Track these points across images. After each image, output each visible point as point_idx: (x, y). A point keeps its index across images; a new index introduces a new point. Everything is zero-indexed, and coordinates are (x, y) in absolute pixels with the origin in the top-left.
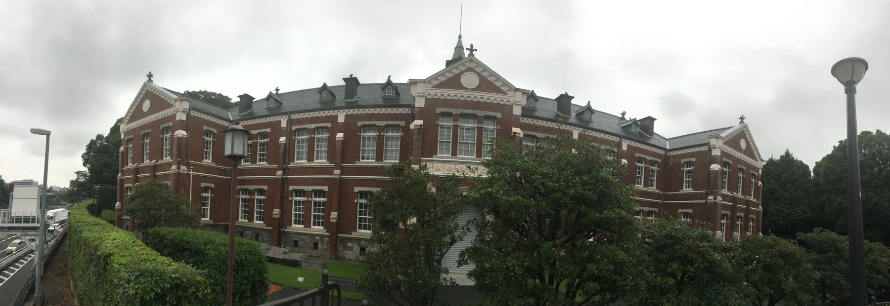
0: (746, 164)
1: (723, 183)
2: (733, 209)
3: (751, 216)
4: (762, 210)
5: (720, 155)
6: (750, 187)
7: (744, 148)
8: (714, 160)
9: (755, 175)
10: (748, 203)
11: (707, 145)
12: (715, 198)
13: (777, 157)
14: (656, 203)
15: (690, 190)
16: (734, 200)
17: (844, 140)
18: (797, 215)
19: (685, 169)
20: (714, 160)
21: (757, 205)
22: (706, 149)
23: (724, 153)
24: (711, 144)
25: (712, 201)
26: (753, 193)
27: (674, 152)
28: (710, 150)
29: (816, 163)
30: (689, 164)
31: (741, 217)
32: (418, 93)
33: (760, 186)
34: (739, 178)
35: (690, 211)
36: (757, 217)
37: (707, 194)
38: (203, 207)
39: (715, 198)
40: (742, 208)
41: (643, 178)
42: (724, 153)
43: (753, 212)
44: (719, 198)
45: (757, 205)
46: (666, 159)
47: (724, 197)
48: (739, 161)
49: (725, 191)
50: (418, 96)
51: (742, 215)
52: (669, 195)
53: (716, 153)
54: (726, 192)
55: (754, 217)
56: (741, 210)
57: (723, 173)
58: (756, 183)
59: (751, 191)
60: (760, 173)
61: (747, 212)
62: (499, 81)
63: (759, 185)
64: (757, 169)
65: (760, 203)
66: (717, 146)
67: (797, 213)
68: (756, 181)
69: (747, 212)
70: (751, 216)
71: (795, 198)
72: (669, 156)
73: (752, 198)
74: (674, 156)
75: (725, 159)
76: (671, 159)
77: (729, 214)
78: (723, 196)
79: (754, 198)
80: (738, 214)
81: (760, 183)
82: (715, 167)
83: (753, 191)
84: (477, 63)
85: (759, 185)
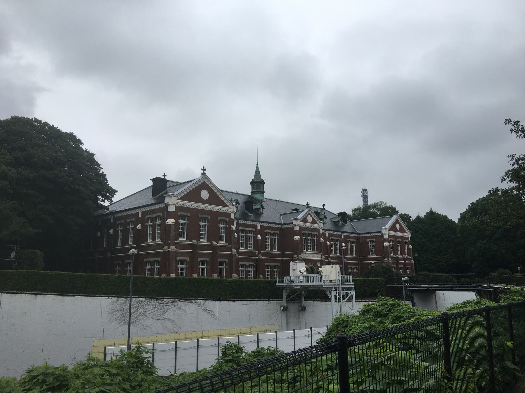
0: (400, 237)
1: (391, 251)
2: (397, 264)
3: (407, 266)
4: (414, 262)
5: (387, 237)
6: (405, 249)
7: (398, 229)
8: (385, 240)
9: (407, 242)
10: (405, 259)
11: (381, 232)
12: (388, 260)
13: (422, 215)
14: (158, 253)
15: (374, 256)
16: (397, 259)
17: (475, 202)
18: (444, 261)
19: (370, 244)
20: (385, 240)
21: (410, 260)
22: (380, 234)
23: (389, 236)
24: (383, 232)
25: (387, 261)
26: (407, 253)
27: (362, 235)
28: (382, 235)
29: (461, 214)
30: (372, 242)
31: (402, 267)
32: (172, 203)
33: (411, 248)
34: (398, 246)
35: (159, 259)
36: (411, 266)
37: (384, 258)
38: (249, 277)
39: (388, 260)
40: (402, 263)
41: (339, 250)
42: (389, 236)
43: (408, 264)
44: (390, 259)
45: (410, 260)
46: (358, 238)
47: (392, 258)
48: (397, 237)
49: (392, 255)
50: (172, 204)
51: (402, 266)
52: (362, 258)
53: (386, 236)
54: (392, 255)
55: (409, 266)
56: (401, 264)
57: (390, 245)
58: (408, 247)
59: (405, 252)
60: (410, 240)
61: (405, 264)
62: (209, 182)
63: (410, 247)
64: (407, 238)
65: (412, 258)
66: (386, 233)
67: (444, 260)
68: (408, 245)
69: (405, 264)
70: (407, 266)
71: (441, 249)
72: (360, 237)
73: (407, 256)
74: (362, 237)
75: (390, 239)
76: (361, 239)
77: (403, 267)
78: (392, 258)
79: (408, 255)
80: (400, 266)
81: (410, 246)
82: (386, 244)
83: (407, 252)
84: (208, 179)
85: (410, 247)
